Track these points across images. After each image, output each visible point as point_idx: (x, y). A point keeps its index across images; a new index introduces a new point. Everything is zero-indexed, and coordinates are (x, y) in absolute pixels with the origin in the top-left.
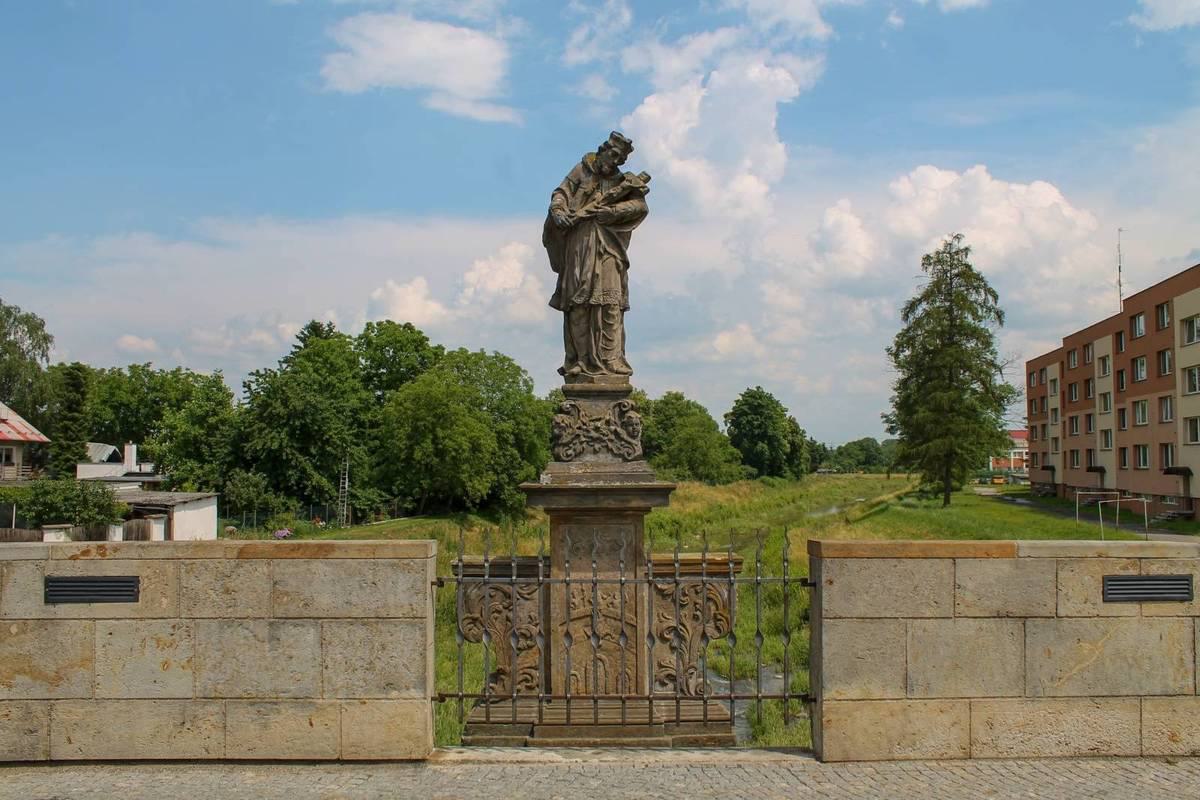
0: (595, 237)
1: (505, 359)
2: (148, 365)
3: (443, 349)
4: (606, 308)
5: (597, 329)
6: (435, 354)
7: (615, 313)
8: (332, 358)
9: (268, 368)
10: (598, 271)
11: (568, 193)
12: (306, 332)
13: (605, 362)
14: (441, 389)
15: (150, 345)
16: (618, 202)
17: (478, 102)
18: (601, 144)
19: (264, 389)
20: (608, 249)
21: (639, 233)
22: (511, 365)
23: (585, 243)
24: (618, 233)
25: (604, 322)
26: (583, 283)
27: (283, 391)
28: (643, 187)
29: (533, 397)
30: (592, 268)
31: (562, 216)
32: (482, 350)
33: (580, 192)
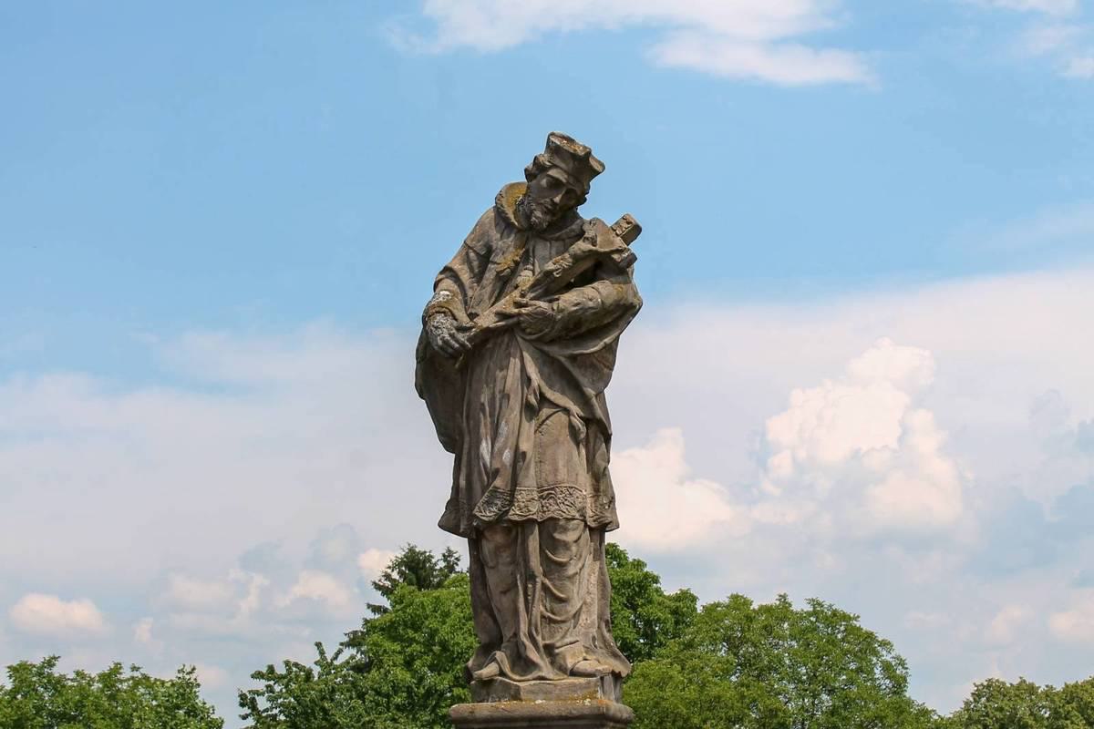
0: (520, 370)
1: (836, 617)
2: (50, 663)
3: (694, 599)
4: (549, 527)
5: (531, 577)
6: (675, 612)
7: (570, 537)
8: (444, 632)
9: (293, 660)
10: (524, 447)
11: (465, 277)
12: (395, 575)
13: (549, 650)
14: (686, 694)
15: (83, 613)
16: (569, 287)
17: (777, 44)
18: (529, 163)
19: (285, 708)
20: (550, 394)
21: (633, 344)
22: (853, 631)
23: (499, 387)
24: (573, 358)
25: (546, 561)
26: (496, 473)
27: (323, 709)
28: (619, 251)
29: (909, 703)
30: (512, 442)
31: (444, 328)
32: (783, 598)
33: (490, 275)
